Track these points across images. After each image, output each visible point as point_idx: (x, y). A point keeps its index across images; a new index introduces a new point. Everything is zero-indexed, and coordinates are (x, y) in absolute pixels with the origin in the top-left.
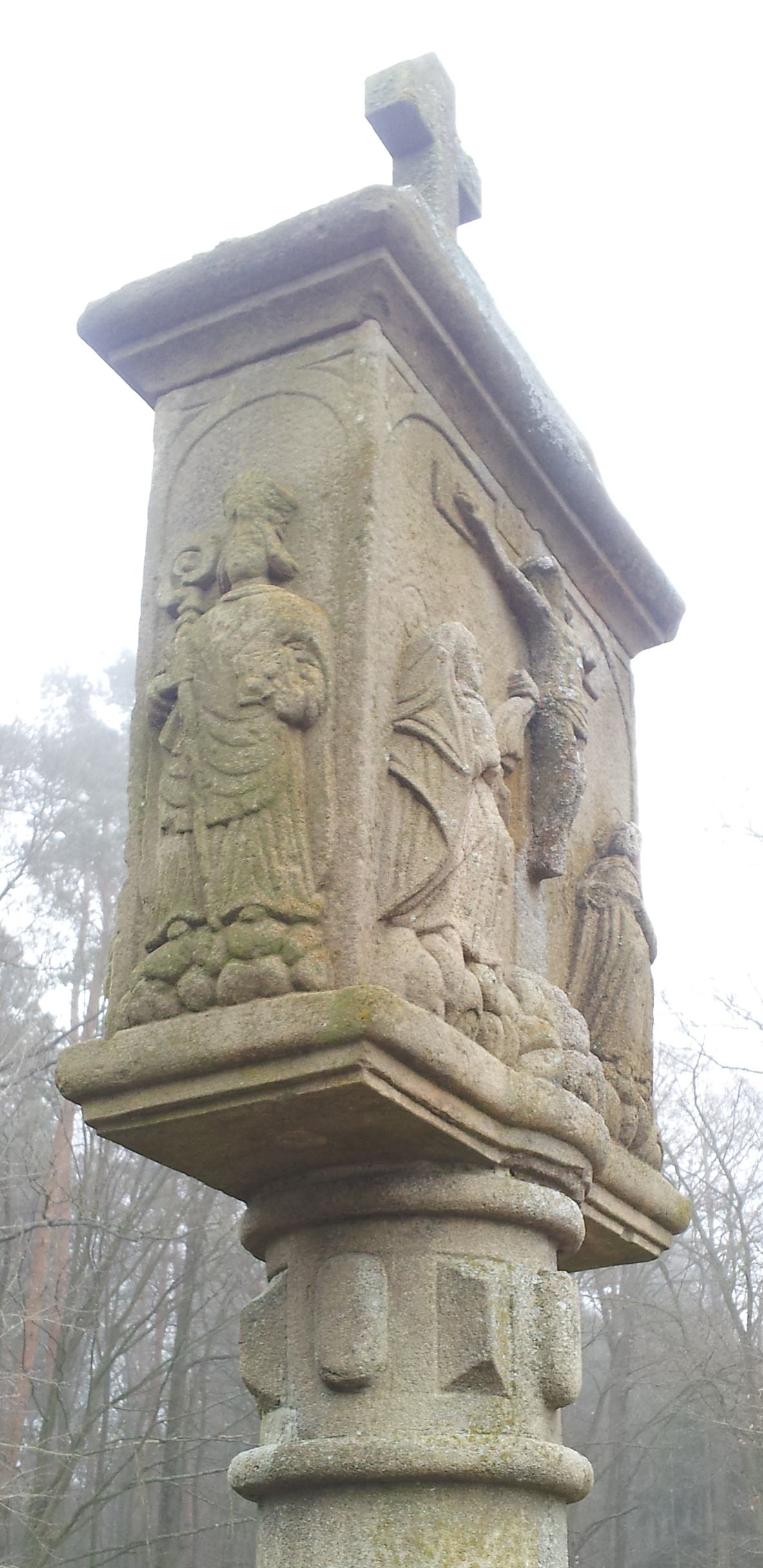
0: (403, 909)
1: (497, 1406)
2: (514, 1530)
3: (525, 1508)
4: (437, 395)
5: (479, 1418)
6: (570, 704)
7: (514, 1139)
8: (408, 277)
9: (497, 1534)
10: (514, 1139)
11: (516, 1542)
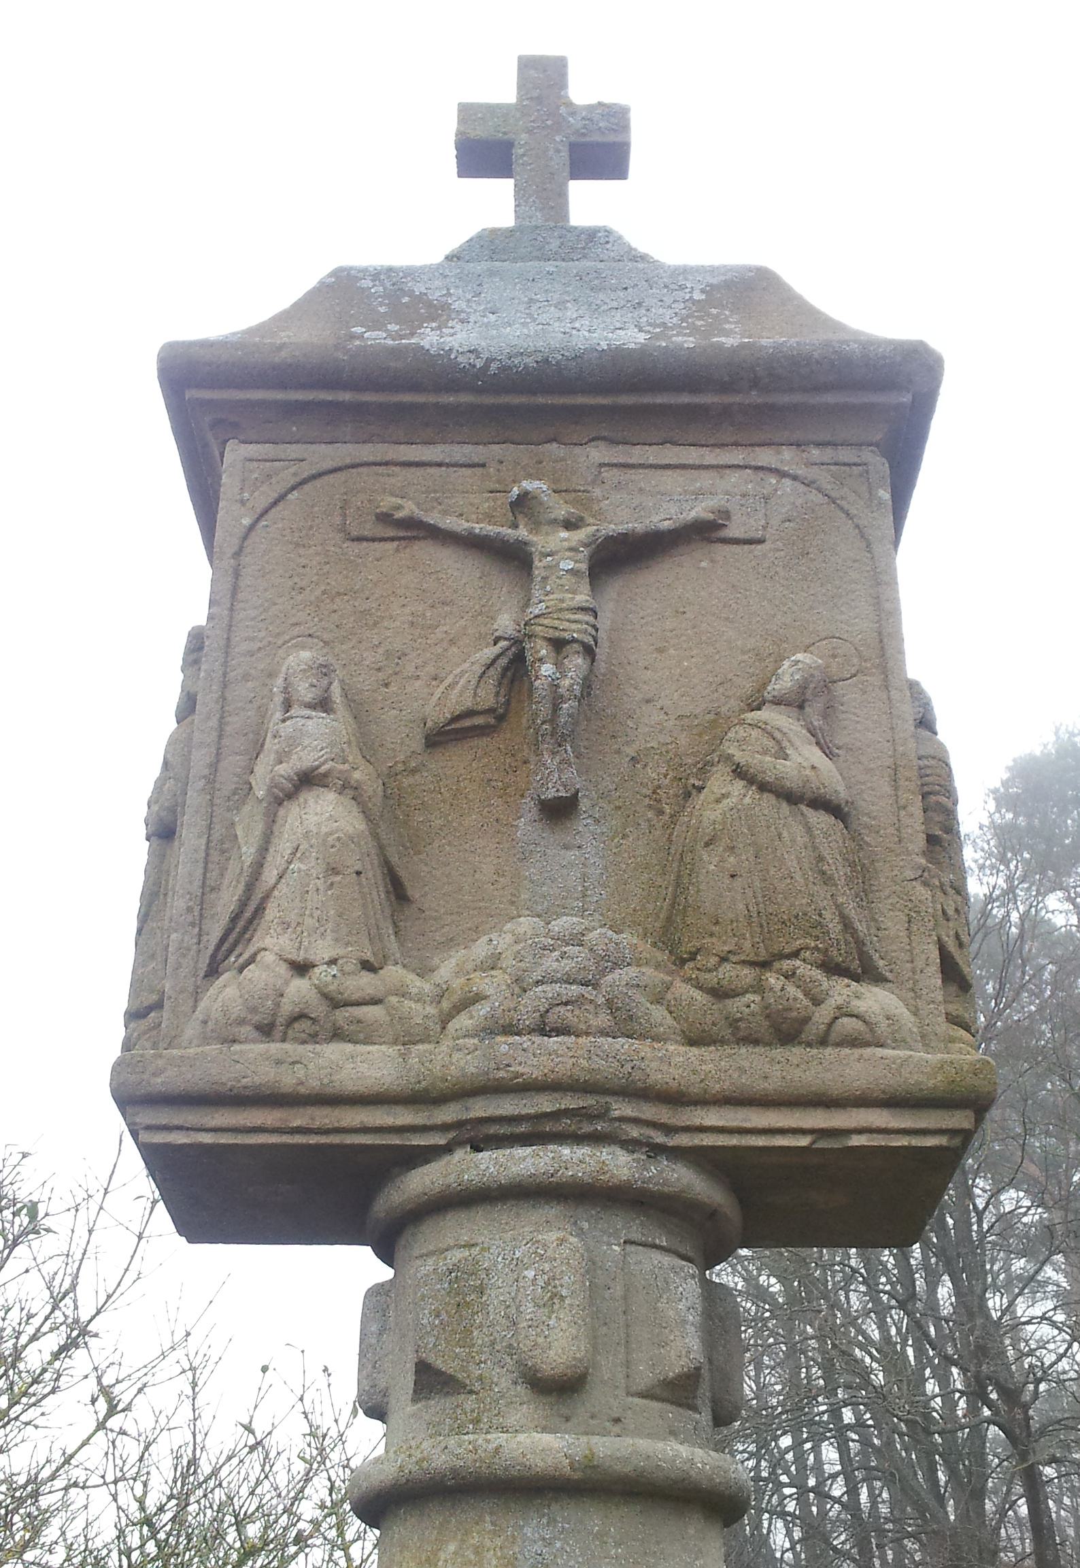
0: (220, 956)
1: (457, 1406)
2: (475, 1539)
3: (491, 1514)
4: (348, 438)
5: (439, 1423)
6: (537, 621)
7: (448, 1114)
8: (229, 387)
9: (452, 1547)
10: (448, 1114)
11: (477, 1553)
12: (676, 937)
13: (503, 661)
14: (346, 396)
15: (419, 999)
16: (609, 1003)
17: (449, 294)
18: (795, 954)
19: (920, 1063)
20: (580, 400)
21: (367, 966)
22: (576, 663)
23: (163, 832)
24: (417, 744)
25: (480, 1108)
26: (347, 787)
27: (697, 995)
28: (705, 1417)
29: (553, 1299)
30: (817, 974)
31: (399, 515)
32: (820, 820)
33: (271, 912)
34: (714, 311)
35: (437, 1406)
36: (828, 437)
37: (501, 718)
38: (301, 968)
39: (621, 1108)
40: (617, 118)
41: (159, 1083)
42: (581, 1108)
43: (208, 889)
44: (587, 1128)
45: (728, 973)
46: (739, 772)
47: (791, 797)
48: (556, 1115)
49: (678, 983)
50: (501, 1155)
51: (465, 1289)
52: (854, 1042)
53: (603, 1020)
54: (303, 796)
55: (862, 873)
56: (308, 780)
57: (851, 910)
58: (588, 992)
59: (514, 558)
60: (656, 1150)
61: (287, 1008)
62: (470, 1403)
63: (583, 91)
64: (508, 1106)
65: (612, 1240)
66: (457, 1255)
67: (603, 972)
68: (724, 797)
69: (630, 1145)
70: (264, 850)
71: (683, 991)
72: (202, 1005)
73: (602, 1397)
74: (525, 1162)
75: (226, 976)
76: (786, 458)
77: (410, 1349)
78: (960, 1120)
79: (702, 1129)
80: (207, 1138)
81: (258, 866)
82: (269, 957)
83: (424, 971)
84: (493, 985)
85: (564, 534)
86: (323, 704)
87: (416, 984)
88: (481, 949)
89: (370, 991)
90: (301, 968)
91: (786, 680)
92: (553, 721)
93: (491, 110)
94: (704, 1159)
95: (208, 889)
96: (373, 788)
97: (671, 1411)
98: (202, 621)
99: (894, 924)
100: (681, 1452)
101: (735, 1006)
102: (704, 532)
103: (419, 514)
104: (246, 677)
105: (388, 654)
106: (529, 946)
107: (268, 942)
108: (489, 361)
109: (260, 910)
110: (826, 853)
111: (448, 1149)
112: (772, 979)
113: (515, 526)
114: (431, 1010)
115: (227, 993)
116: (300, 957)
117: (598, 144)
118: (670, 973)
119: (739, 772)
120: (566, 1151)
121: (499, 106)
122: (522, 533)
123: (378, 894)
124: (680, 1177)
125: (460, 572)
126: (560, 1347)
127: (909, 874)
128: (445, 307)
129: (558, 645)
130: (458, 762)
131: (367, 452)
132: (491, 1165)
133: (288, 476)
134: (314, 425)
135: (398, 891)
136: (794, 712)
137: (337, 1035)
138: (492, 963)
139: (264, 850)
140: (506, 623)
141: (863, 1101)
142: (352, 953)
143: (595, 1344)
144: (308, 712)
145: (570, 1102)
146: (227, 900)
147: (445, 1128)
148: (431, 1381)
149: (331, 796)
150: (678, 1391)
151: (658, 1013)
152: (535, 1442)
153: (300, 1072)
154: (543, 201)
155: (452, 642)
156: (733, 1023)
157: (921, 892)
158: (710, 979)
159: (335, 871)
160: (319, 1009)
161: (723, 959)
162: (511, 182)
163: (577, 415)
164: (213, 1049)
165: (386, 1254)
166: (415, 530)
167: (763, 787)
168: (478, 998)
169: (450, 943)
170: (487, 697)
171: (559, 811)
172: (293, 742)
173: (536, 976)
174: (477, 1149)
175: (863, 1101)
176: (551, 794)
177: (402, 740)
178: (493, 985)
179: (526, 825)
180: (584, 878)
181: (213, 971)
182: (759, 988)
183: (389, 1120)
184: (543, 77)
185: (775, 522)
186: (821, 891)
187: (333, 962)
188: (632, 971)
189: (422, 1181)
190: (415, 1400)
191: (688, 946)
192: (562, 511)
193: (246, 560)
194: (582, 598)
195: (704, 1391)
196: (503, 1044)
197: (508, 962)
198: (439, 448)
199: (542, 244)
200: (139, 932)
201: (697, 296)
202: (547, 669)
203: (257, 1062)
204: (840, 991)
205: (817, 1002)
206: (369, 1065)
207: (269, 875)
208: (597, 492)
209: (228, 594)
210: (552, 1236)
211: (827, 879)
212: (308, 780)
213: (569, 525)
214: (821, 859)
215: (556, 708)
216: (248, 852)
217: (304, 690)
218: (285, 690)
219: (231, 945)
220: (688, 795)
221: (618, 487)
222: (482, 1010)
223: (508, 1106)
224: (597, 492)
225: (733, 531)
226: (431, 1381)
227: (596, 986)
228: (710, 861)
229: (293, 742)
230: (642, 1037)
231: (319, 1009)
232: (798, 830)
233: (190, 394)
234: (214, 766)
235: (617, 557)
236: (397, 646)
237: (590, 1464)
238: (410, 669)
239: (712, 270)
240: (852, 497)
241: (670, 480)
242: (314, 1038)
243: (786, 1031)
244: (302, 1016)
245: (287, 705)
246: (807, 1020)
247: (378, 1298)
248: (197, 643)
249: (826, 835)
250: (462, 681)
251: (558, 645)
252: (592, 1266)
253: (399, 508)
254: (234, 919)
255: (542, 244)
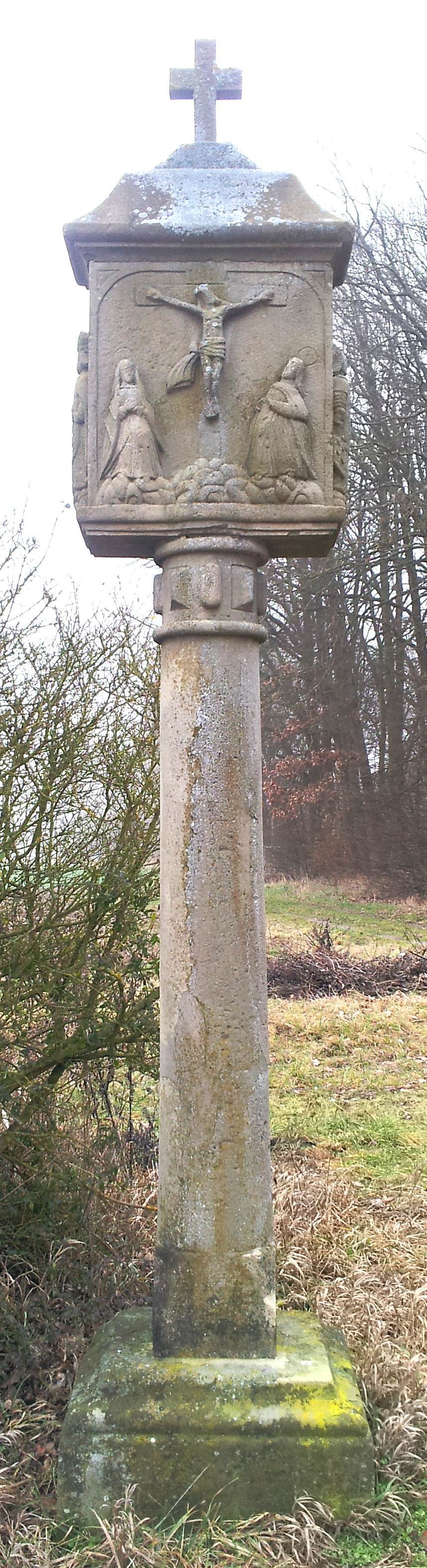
7: (178, 527)
10: (178, 527)
12: (248, 464)
13: (193, 361)
14: (133, 245)
15: (169, 489)
16: (228, 491)
17: (169, 189)
18: (286, 474)
19: (321, 509)
20: (221, 246)
21: (152, 479)
22: (219, 364)
23: (80, 422)
24: (164, 393)
25: (188, 526)
26: (143, 415)
27: (254, 487)
28: (254, 614)
29: (210, 583)
30: (293, 480)
31: (155, 297)
32: (297, 425)
33: (121, 460)
34: (272, 199)
35: (177, 612)
36: (311, 259)
37: (192, 383)
38: (132, 479)
39: (231, 525)
40: (236, 76)
41: (91, 517)
42: (218, 526)
43: (98, 448)
44: (220, 532)
45: (264, 480)
46: (271, 408)
48: (211, 528)
49: (249, 483)
50: (195, 540)
51: (185, 580)
52: (303, 502)
53: (226, 497)
54: (129, 417)
55: (310, 440)
56: (130, 412)
57: (305, 457)
58: (221, 488)
59: (197, 317)
60: (241, 538)
61: (128, 493)
62: (187, 611)
63: (223, 62)
64: (197, 525)
65: (215, 654)
66: (183, 569)
67: (226, 480)
68: (266, 418)
69: (233, 536)
70: (117, 438)
71: (251, 486)
72: (101, 489)
73: (223, 610)
74: (202, 542)
75: (107, 480)
76: (295, 268)
77: (169, 595)
78: (334, 527)
79: (255, 530)
80: (106, 534)
81: (116, 444)
82: (121, 476)
83: (169, 478)
84: (192, 485)
85: (214, 310)
86: (133, 382)
87: (168, 484)
88: (187, 472)
89: (154, 488)
90: (132, 479)
91: (287, 372)
92: (210, 388)
93: (183, 72)
94: (258, 540)
95: (98, 448)
96: (151, 415)
97: (244, 613)
98: (87, 331)
99: (319, 459)
100: (248, 625)
101: (267, 492)
102: (264, 303)
103: (162, 297)
104: (104, 365)
105: (153, 355)
106: (204, 469)
107: (121, 470)
108: (187, 231)
109: (117, 458)
110: (298, 437)
111: (179, 537)
112: (279, 483)
113: (197, 304)
114: (172, 493)
115: (108, 487)
116: (132, 476)
117: (228, 91)
118: (247, 479)
119: (271, 408)
120: (214, 539)
121: (187, 70)
122: (198, 308)
123: (154, 453)
124: (248, 545)
125: (177, 320)
126: (212, 596)
127: (326, 441)
128: (168, 196)
129: (212, 358)
130: (178, 400)
131: (142, 266)
133: (114, 277)
134: (122, 252)
135: (160, 450)
136: (291, 382)
137: (144, 501)
138: (191, 477)
139: (117, 438)
140: (193, 346)
141: (304, 521)
142: (148, 475)
143: (222, 596)
144: (128, 386)
146: (106, 454)
147: (178, 531)
148: (175, 605)
149: (138, 418)
150: (246, 608)
151: (243, 494)
152: (206, 623)
153: (133, 514)
154: (206, 120)
155: (175, 350)
156: (266, 497)
157: (330, 447)
158: (259, 482)
159: (141, 447)
160: (138, 493)
161: (263, 476)
162: (192, 101)
163: (217, 251)
164: (106, 506)
165: (159, 563)
166: (160, 303)
167: (279, 414)
168: (187, 490)
169: (177, 467)
170: (188, 376)
171: (212, 420)
172: (124, 397)
173: (205, 482)
174: (188, 537)
175: (304, 521)
176: (209, 415)
177: (159, 392)
178: (192, 485)
179: (201, 424)
180: (221, 443)
181: (103, 478)
182: (274, 485)
183: (161, 529)
184: (205, 52)
185: (290, 297)
186: (296, 451)
187: (142, 478)
188: (235, 480)
189: (172, 546)
190: (172, 609)
191: (253, 470)
192: (214, 298)
193: (101, 315)
194: (220, 339)
195: (255, 607)
196: (195, 506)
197: (196, 477)
198: (169, 264)
199: (205, 155)
200: (74, 457)
201: (266, 190)
202: (208, 369)
203: (120, 510)
204: (300, 485)
205: (292, 490)
206: (154, 511)
207: (120, 447)
208: (226, 283)
210: (210, 565)
211: (298, 447)
212: (130, 412)
213: (216, 304)
214: (296, 439)
215: (211, 383)
216: (112, 438)
217: (126, 377)
218: (120, 375)
219: (108, 471)
220: (255, 412)
221: (234, 281)
222: (188, 494)
223: (197, 525)
224: (226, 283)
225: (275, 302)
226: (175, 605)
227: (223, 485)
228: (260, 442)
229: (124, 397)
230: (238, 502)
231: (138, 493)
232: (290, 429)
234: (96, 401)
235: (232, 316)
236: (157, 352)
237: (220, 628)
238: (160, 361)
239: (272, 175)
240: (319, 286)
241: (253, 278)
242: (137, 503)
243: (281, 499)
244: (133, 496)
245: (121, 381)
246: (289, 496)
247: (157, 577)
248: (84, 343)
249: (299, 430)
250: (178, 371)
251: (212, 358)
253: (155, 294)
254: (109, 462)
255: (205, 155)
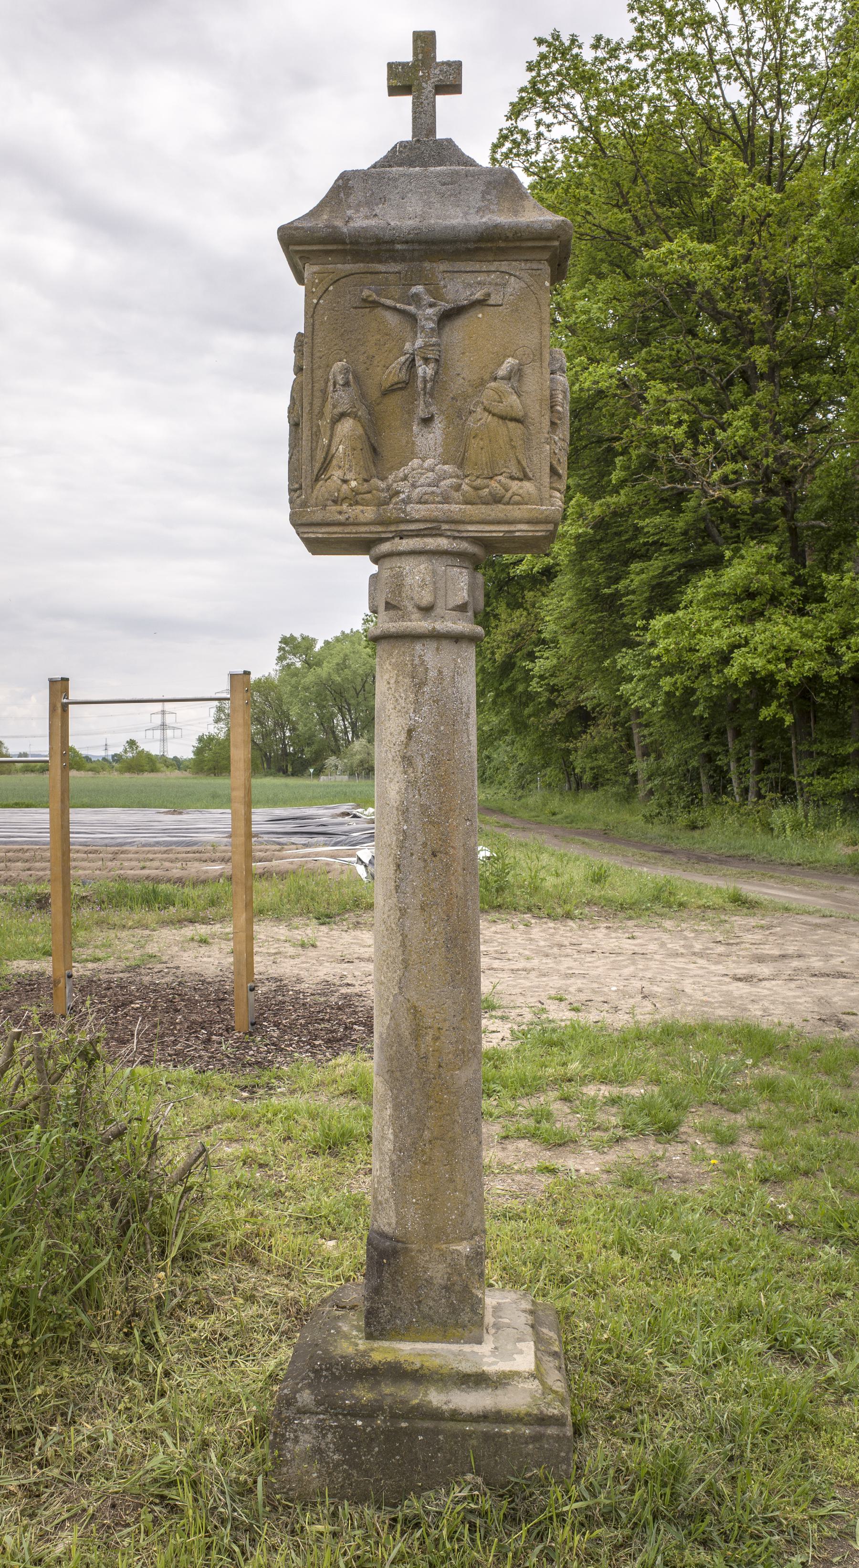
7: (393, 528)
21: (366, 481)
26: (355, 417)
33: (334, 462)
35: (392, 613)
47: (503, 418)
56: (343, 415)
60: (455, 538)
65: (440, 566)
69: (448, 537)
70: (330, 441)
73: (438, 611)
83: (383, 479)
90: (345, 481)
91: (502, 372)
97: (458, 614)
102: (481, 303)
124: (464, 546)
126: (426, 598)
132: (406, 544)
135: (374, 450)
145: (429, 525)
146: (320, 455)
152: (419, 624)
169: (392, 469)
175: (520, 522)
181: (317, 479)
199: (425, 150)
203: (332, 512)
209: (312, 312)
225: (491, 302)
233: (291, 248)
243: (497, 500)
247: (374, 579)
252: (434, 573)
